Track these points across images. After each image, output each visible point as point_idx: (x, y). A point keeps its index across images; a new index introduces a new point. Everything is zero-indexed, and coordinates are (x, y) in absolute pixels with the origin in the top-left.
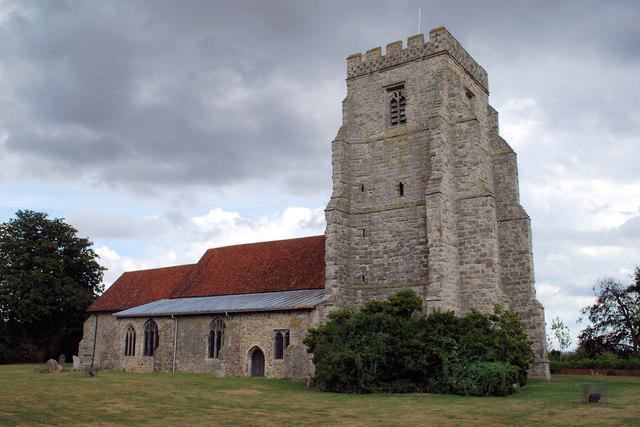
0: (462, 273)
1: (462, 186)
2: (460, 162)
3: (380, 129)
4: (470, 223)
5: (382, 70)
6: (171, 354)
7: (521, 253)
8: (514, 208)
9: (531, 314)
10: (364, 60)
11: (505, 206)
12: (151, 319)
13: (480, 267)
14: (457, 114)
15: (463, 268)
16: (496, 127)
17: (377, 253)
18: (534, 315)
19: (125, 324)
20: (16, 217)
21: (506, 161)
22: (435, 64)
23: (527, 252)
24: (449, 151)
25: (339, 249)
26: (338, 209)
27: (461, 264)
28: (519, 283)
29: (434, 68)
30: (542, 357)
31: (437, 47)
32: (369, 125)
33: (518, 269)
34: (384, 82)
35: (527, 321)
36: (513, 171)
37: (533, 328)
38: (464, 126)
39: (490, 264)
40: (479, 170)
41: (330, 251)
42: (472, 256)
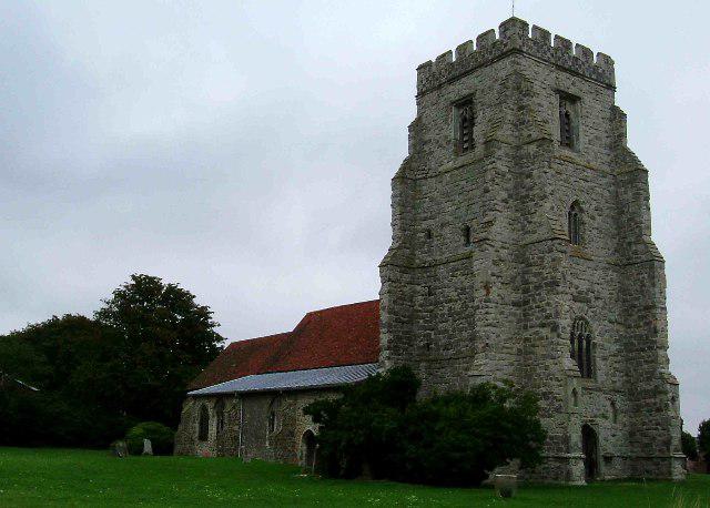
0: (526, 340)
1: (529, 227)
2: (527, 196)
3: (445, 159)
4: (535, 275)
5: (451, 81)
6: (236, 439)
7: (648, 308)
8: (640, 247)
9: (657, 392)
10: (434, 68)
11: (630, 244)
12: (220, 398)
13: (545, 332)
14: (525, 133)
15: (526, 335)
16: (622, 136)
17: (443, 315)
18: (660, 392)
19: (199, 404)
20: (122, 288)
21: (630, 182)
22: (504, 68)
23: (654, 307)
24: (510, 185)
25: (395, 313)
26: (397, 266)
27: (525, 327)
28: (643, 350)
29: (503, 74)
30: (668, 449)
31: (505, 45)
32: (438, 153)
33: (642, 331)
34: (453, 97)
35: (653, 400)
36: (642, 195)
37: (659, 410)
38: (532, 148)
39: (555, 328)
40: (547, 205)
41: (384, 317)
42: (538, 318)
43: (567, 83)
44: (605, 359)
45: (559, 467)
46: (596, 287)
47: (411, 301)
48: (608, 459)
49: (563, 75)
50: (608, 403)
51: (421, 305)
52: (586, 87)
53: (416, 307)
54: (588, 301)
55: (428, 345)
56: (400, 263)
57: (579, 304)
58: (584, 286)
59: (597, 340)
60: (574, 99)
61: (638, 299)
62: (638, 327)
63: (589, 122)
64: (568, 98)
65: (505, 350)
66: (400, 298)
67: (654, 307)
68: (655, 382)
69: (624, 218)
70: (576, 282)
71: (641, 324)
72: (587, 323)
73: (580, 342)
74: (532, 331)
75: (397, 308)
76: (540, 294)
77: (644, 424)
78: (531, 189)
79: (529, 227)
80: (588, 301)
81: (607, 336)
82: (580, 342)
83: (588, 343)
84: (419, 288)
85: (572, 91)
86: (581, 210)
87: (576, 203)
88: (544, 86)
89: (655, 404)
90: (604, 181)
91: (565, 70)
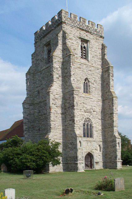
5: (44, 37)
18: (114, 141)
28: (109, 128)
34: (44, 43)
43: (84, 35)
44: (97, 131)
45: (75, 166)
46: (94, 108)
47: (33, 115)
48: (97, 163)
49: (82, 32)
50: (98, 145)
51: (37, 116)
52: (92, 37)
53: (35, 117)
54: (90, 112)
55: (39, 129)
56: (29, 102)
57: (87, 113)
58: (89, 107)
59: (94, 125)
60: (87, 41)
61: (108, 111)
62: (108, 120)
63: (93, 50)
64: (84, 41)
65: (58, 129)
66: (29, 114)
67: (30, 105)
68: (113, 138)
69: (105, 83)
70: (86, 106)
71: (109, 119)
72: (90, 119)
73: (87, 126)
74: (67, 122)
75: (28, 117)
76: (69, 110)
77: (109, 151)
78: (67, 73)
79: (66, 87)
80: (90, 112)
81: (97, 124)
82: (87, 126)
83: (91, 126)
84: (36, 111)
85: (86, 38)
86: (89, 81)
87: (86, 79)
88: (75, 36)
89: (113, 145)
90: (97, 71)
91: (83, 30)
